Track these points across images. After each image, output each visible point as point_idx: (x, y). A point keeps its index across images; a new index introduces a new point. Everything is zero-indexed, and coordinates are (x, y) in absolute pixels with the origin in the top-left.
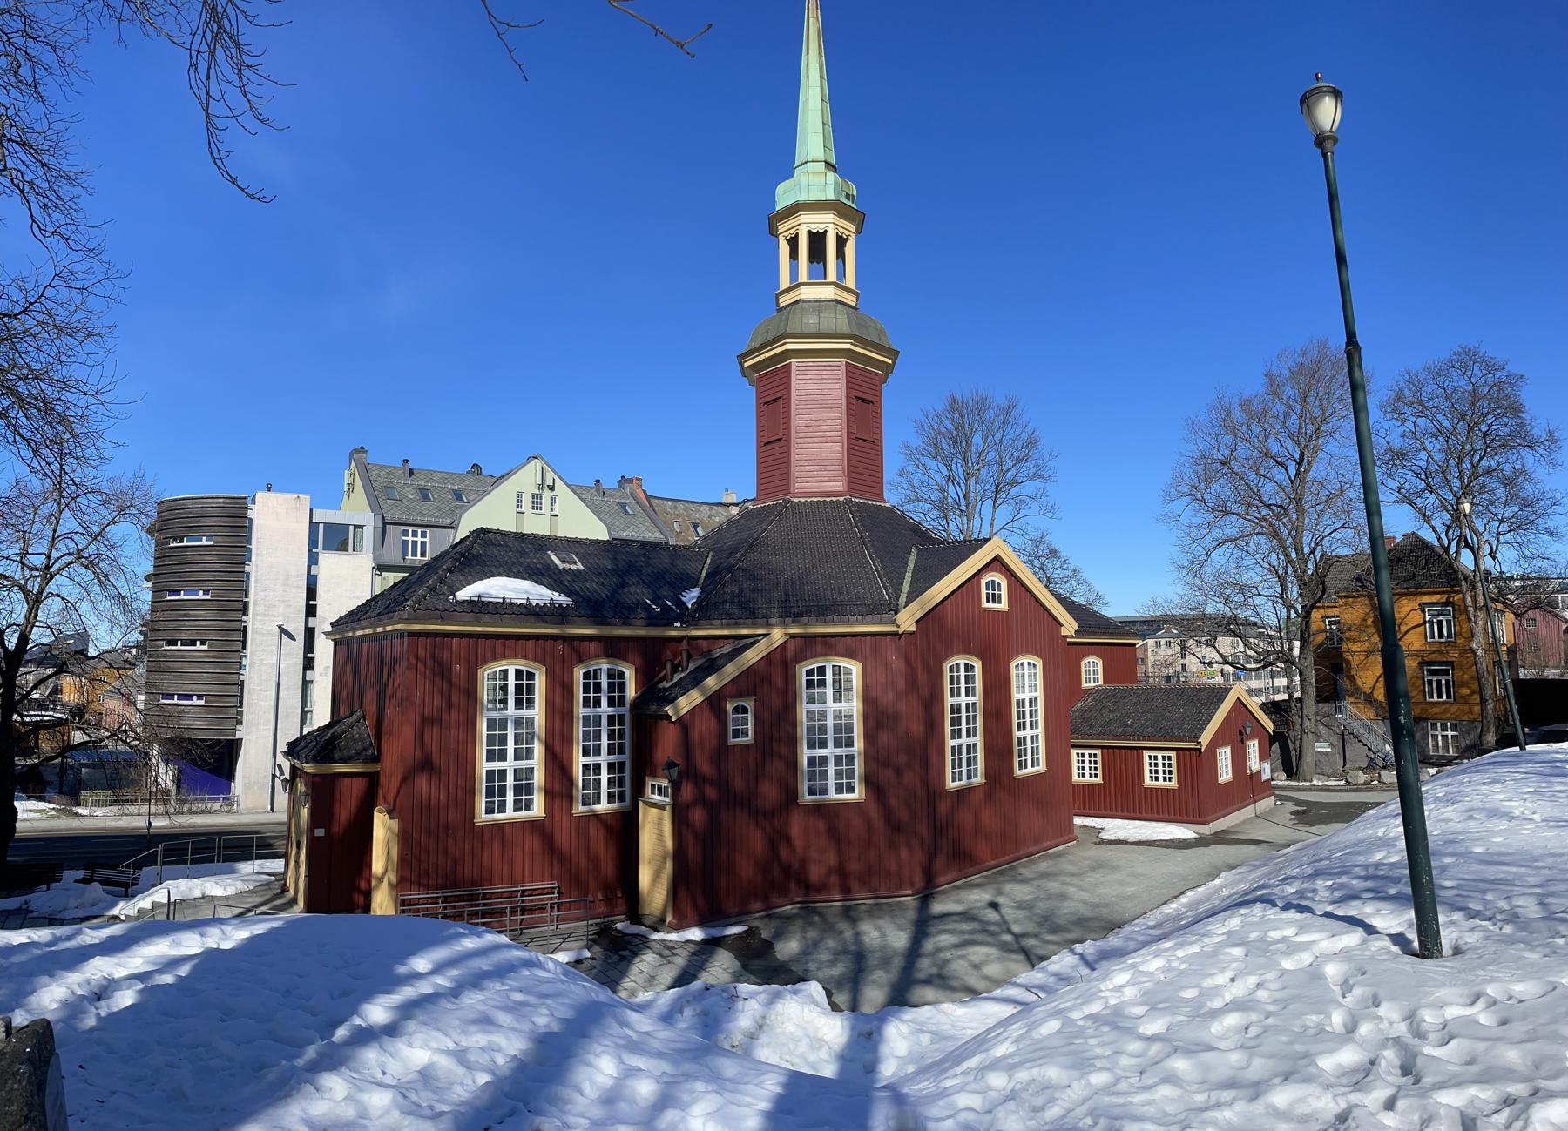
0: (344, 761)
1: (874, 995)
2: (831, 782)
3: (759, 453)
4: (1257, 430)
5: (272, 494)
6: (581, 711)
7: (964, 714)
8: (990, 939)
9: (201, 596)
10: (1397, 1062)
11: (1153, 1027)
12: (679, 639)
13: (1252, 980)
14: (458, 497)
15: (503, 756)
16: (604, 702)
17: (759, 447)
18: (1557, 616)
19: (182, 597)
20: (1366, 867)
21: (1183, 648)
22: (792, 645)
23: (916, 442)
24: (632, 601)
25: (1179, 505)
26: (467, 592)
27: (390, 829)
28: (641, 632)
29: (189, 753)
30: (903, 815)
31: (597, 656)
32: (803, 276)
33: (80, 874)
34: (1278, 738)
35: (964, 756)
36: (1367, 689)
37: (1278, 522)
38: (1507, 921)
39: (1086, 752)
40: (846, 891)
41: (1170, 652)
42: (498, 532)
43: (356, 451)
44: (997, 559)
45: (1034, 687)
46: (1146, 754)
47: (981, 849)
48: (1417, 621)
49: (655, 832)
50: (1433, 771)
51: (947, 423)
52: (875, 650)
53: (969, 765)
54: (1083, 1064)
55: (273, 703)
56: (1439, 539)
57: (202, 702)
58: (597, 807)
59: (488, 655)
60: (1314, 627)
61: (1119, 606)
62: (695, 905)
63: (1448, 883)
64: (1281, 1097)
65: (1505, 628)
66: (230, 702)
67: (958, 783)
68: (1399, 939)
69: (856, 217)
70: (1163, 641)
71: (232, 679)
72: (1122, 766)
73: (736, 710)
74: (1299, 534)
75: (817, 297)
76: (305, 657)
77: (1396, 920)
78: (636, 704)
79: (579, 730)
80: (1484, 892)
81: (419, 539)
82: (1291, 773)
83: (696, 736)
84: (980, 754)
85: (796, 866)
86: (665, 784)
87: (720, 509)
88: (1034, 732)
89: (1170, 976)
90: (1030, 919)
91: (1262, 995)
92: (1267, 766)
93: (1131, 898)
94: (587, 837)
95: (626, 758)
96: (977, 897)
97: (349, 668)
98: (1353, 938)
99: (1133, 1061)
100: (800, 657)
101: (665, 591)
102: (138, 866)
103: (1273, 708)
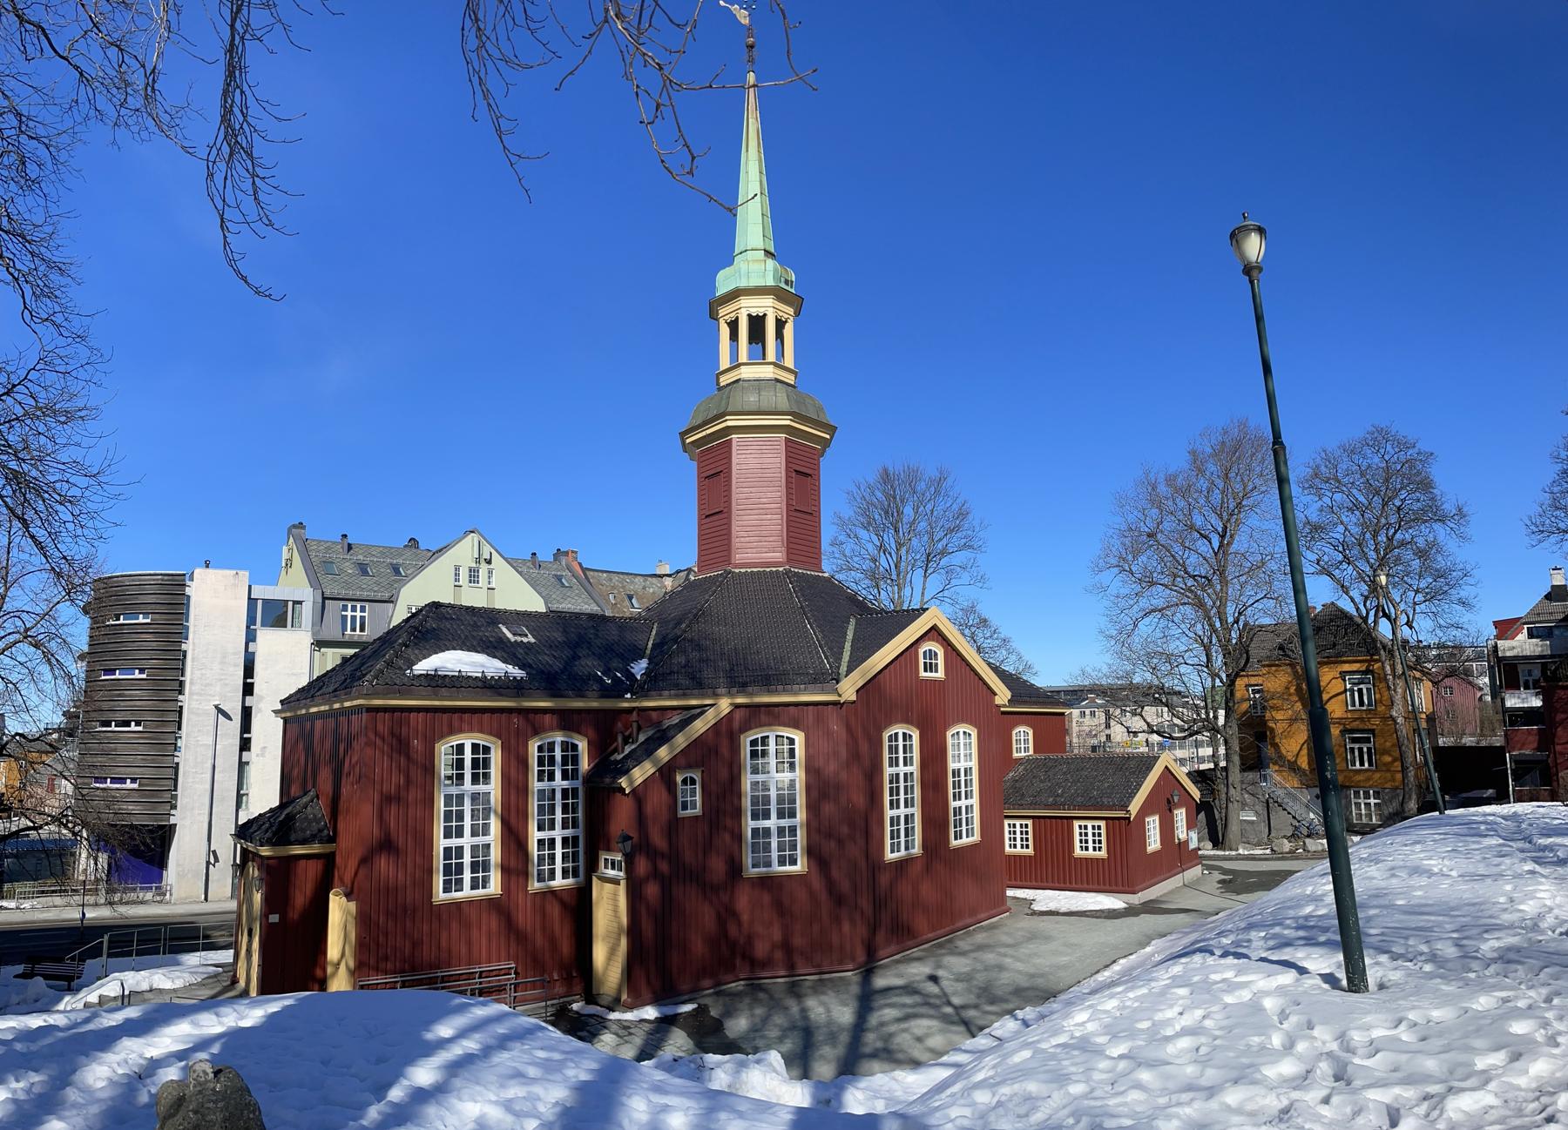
0: (303, 842)
1: (825, 1069)
2: (775, 854)
3: (700, 525)
4: (1181, 504)
5: (209, 571)
6: (536, 785)
7: (902, 784)
8: (932, 1012)
9: (137, 675)
10: (1330, 1072)
11: (1115, 1052)
12: (630, 711)
13: (1199, 1013)
14: (396, 570)
15: (460, 834)
16: (558, 775)
17: (700, 519)
18: (1470, 683)
19: (117, 676)
20: (1296, 918)
21: (1108, 717)
22: (738, 715)
23: (848, 512)
24: (583, 672)
25: (1107, 577)
26: (424, 666)
27: (347, 912)
28: (595, 704)
29: (132, 838)
30: (845, 886)
31: (552, 729)
32: (743, 358)
33: (20, 969)
34: (1204, 807)
35: (902, 827)
36: (1290, 757)
37: (1203, 591)
38: (1426, 961)
39: (1018, 823)
40: (791, 968)
41: (1096, 721)
42: (506, 611)
43: (294, 526)
44: (934, 628)
45: (968, 757)
46: (1076, 824)
47: (920, 922)
48: (1340, 689)
49: (610, 906)
50: (1356, 839)
51: (879, 494)
52: (819, 720)
53: (907, 835)
54: (1061, 1079)
55: (208, 787)
56: (1358, 609)
57: (135, 786)
58: (552, 883)
59: (445, 729)
60: (1238, 695)
61: (1048, 675)
62: (649, 982)
63: (1373, 931)
64: (1233, 1097)
65: (1423, 696)
66: (165, 785)
67: (896, 855)
68: (1329, 979)
69: (796, 301)
70: (1088, 711)
71: (167, 762)
72: (1053, 835)
73: (684, 782)
74: (1223, 604)
75: (757, 376)
76: (242, 738)
77: (1329, 962)
78: (589, 779)
79: (534, 805)
80: (1407, 938)
81: (358, 614)
82: (1217, 843)
83: (649, 809)
84: (917, 824)
85: (742, 941)
86: (619, 857)
87: (654, 580)
88: (969, 802)
89: (1125, 1012)
90: (969, 991)
91: (1208, 1023)
92: (1194, 836)
93: (1065, 967)
94: (544, 915)
95: (580, 832)
96: (917, 971)
97: (301, 746)
98: (1288, 977)
99: (1104, 1076)
100: (745, 728)
101: (615, 663)
102: (83, 958)
103: (1199, 777)
